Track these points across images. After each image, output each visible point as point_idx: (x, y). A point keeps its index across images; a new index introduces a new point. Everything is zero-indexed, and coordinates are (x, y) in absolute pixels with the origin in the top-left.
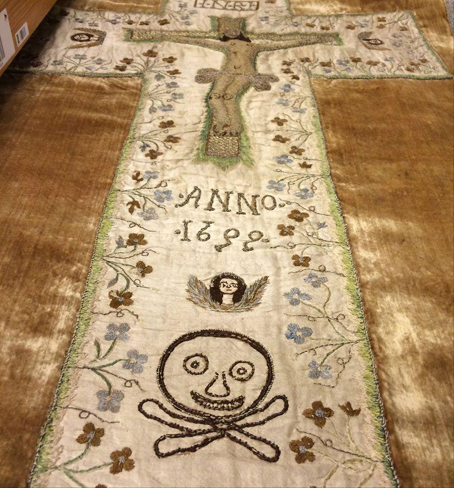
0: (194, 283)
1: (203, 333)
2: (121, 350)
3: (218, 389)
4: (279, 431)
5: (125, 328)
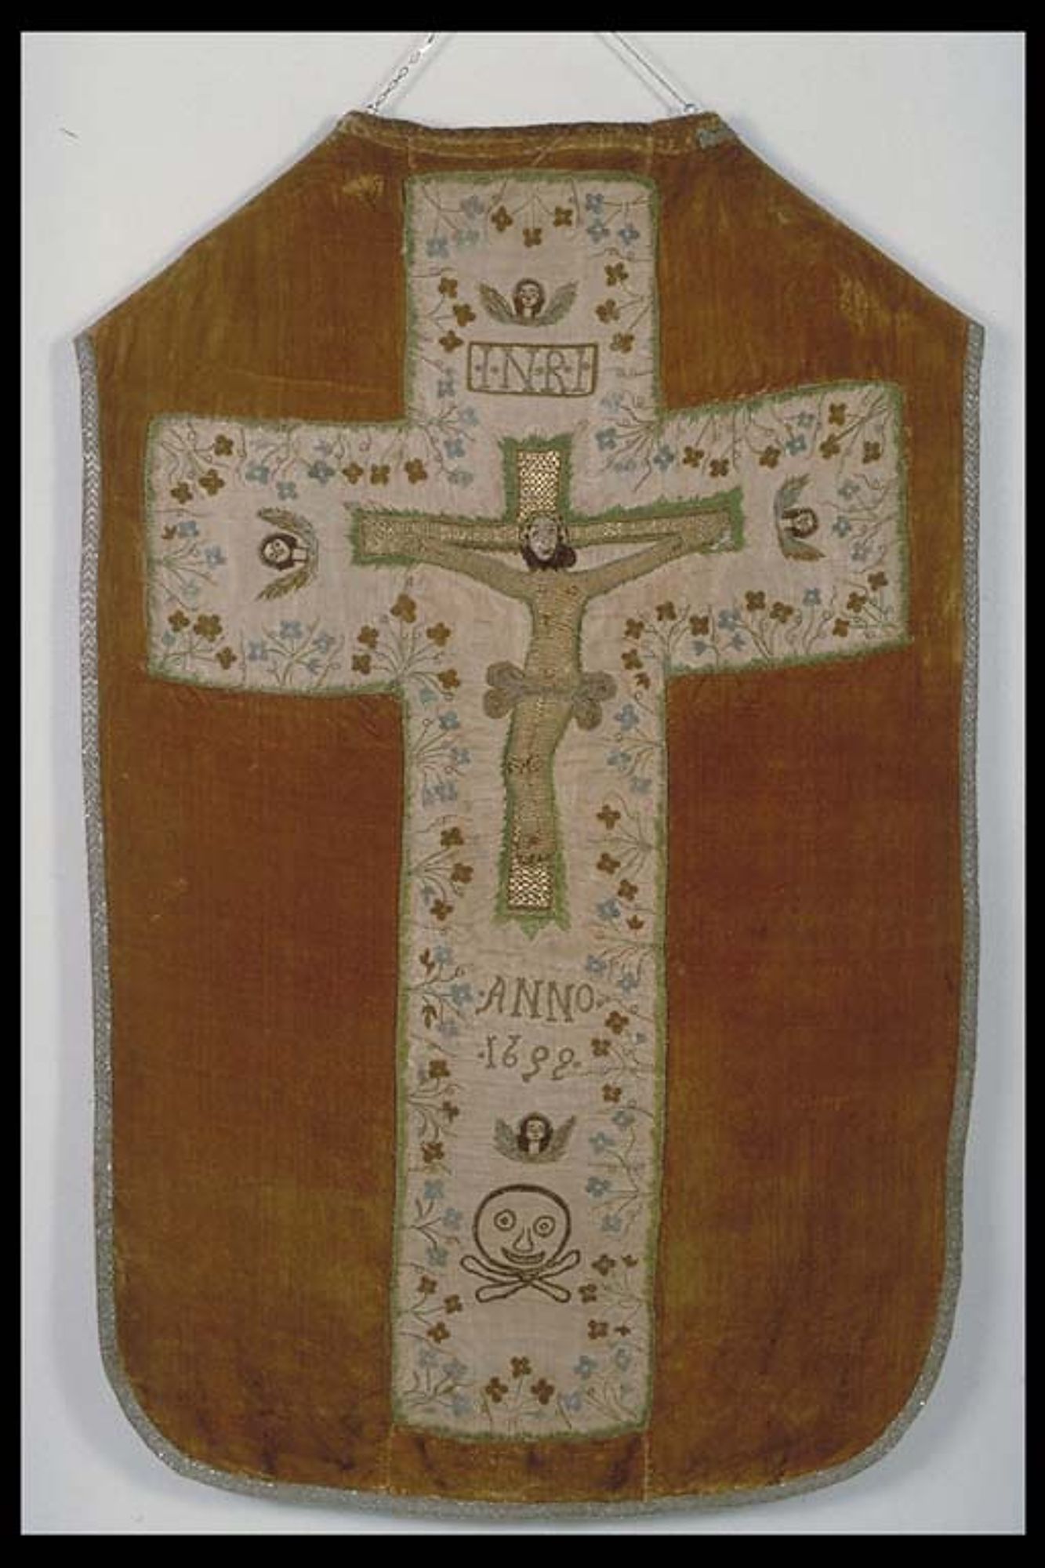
0: (502, 1126)
2: (439, 1210)
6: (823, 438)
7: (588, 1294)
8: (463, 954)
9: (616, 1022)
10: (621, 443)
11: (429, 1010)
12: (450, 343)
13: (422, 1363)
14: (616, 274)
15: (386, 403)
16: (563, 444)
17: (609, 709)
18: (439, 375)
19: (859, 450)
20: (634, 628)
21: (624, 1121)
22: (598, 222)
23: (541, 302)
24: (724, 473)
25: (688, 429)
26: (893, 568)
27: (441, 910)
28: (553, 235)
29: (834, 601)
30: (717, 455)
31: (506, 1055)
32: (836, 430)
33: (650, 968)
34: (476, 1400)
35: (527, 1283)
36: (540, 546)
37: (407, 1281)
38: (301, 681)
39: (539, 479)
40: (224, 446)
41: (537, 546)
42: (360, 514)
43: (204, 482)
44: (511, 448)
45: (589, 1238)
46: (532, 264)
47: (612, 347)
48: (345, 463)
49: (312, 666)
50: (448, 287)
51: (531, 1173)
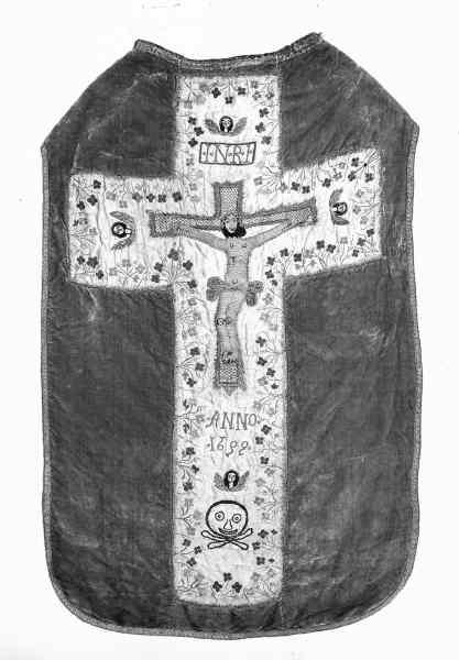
0: (217, 475)
1: (222, 502)
2: (191, 512)
3: (228, 527)
4: (250, 540)
5: (191, 501)
6: (349, 173)
7: (256, 546)
8: (200, 401)
9: (266, 430)
10: (264, 182)
11: (186, 426)
12: (193, 143)
13: (185, 575)
14: (263, 113)
15: (165, 169)
16: (240, 185)
17: (261, 297)
18: (186, 156)
19: (364, 178)
20: (271, 261)
21: (270, 473)
22: (257, 93)
23: (232, 126)
24: (308, 191)
25: (290, 177)
26: (377, 227)
27: (191, 383)
28: (239, 99)
29: (349, 243)
30: (305, 184)
31: (218, 446)
32: (354, 169)
33: (280, 405)
34: (210, 590)
35: (230, 542)
36: (231, 226)
37: (178, 541)
38: (131, 285)
39: (229, 197)
40: (97, 185)
41: (227, 226)
42: (152, 216)
43: (89, 200)
44: (217, 187)
45: (257, 523)
46: (229, 110)
47: (262, 142)
48: (148, 194)
49: (135, 279)
50: (192, 121)
51: (229, 495)
